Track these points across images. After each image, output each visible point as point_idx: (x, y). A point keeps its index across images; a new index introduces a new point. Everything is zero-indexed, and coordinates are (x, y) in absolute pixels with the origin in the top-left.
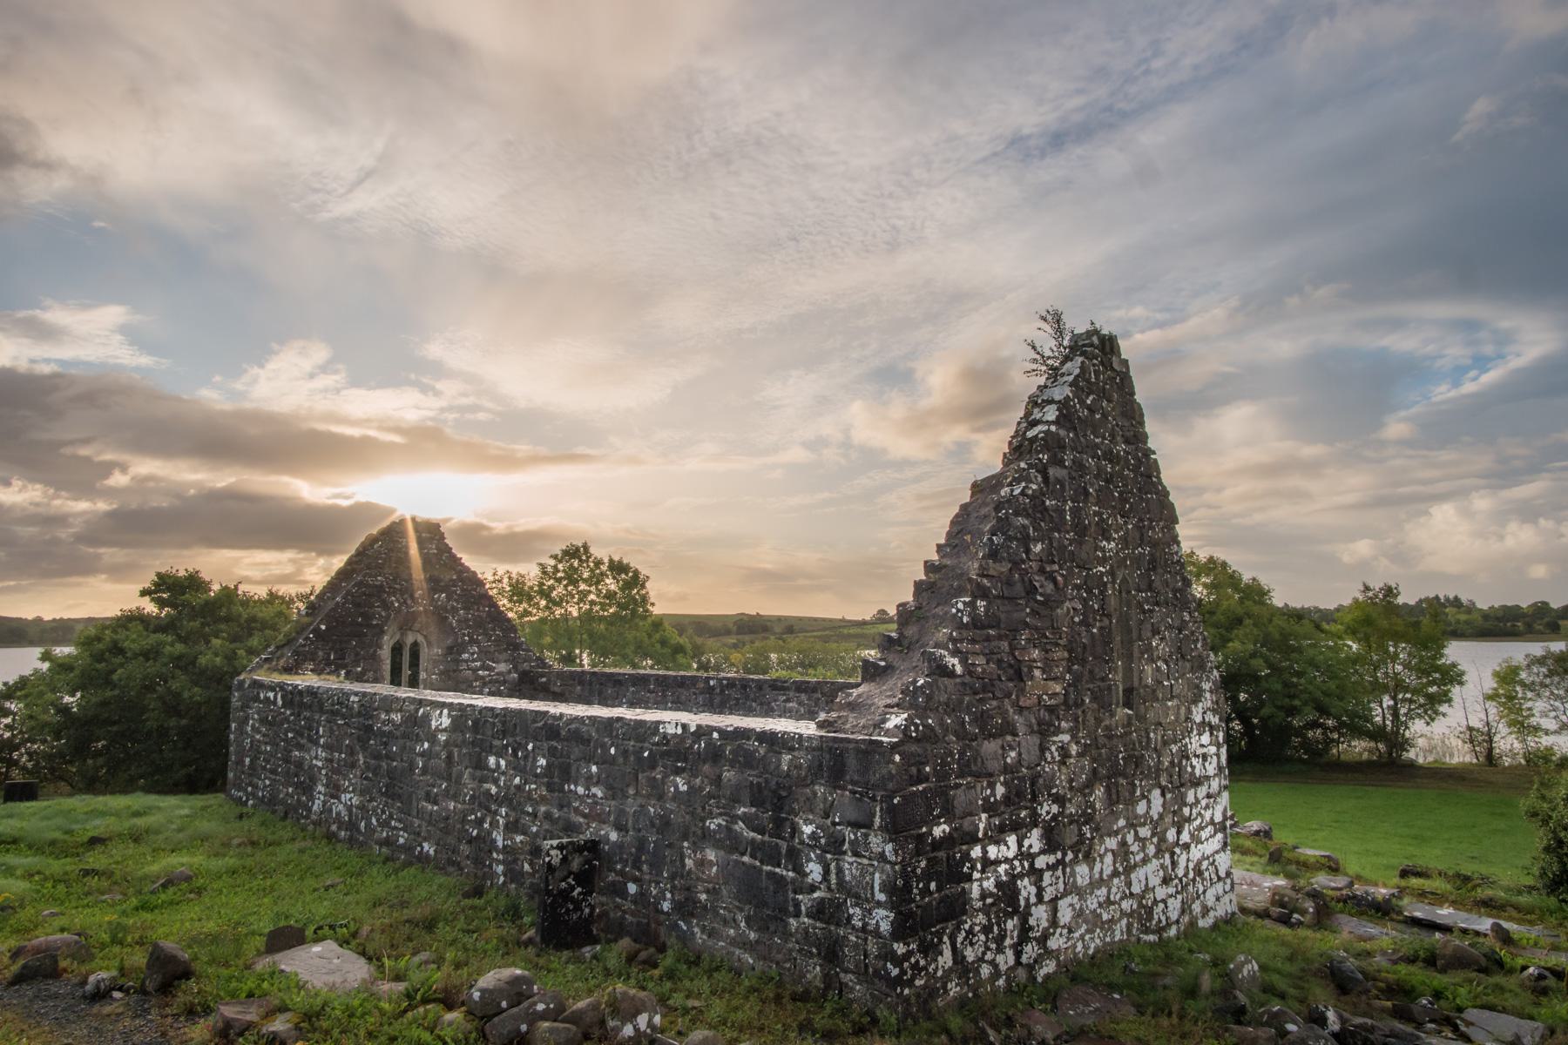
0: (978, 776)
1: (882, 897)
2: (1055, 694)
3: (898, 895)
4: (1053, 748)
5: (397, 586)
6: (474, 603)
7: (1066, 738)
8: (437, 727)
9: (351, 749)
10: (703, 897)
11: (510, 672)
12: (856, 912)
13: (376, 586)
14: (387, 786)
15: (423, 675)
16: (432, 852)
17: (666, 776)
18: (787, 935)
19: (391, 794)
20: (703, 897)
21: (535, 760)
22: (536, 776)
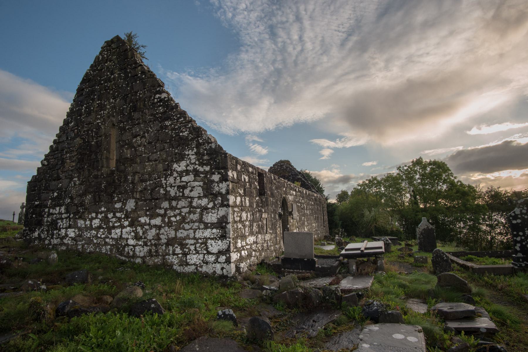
4: (72, 183)
7: (76, 179)
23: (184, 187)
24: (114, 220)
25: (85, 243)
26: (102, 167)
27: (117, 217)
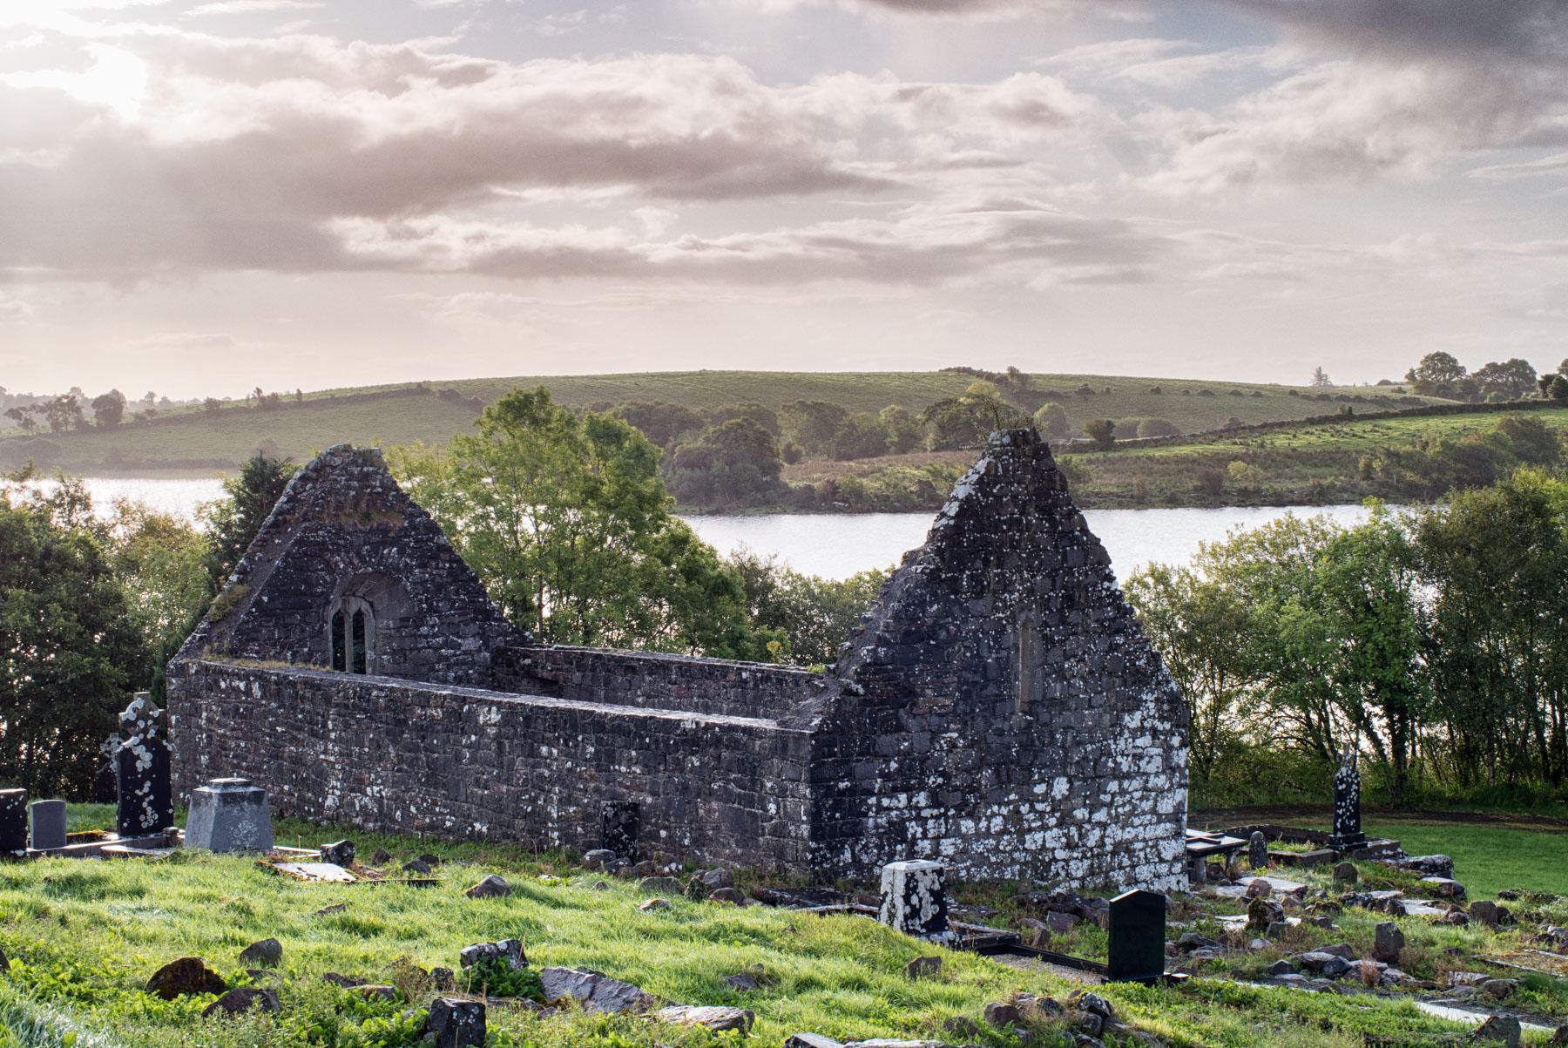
0: (876, 755)
1: (804, 818)
2: (944, 706)
3: (815, 817)
5: (341, 542)
6: (430, 558)
8: (485, 722)
9: (378, 742)
10: (710, 833)
11: (479, 650)
12: (792, 828)
13: (318, 543)
14: (427, 776)
15: (370, 655)
16: (484, 829)
17: (685, 757)
18: (758, 847)
19: (432, 781)
20: (710, 833)
21: (584, 747)
22: (586, 760)
23: (1141, 757)
24: (1031, 816)
25: (972, 865)
26: (1013, 713)
27: (1036, 812)
